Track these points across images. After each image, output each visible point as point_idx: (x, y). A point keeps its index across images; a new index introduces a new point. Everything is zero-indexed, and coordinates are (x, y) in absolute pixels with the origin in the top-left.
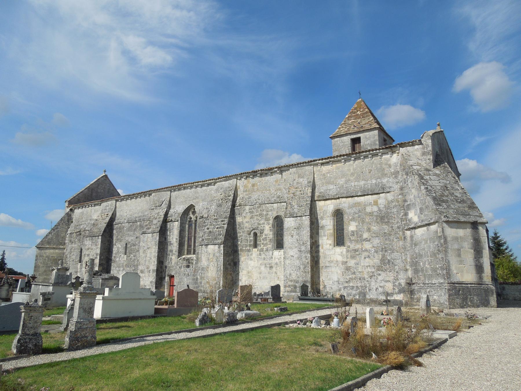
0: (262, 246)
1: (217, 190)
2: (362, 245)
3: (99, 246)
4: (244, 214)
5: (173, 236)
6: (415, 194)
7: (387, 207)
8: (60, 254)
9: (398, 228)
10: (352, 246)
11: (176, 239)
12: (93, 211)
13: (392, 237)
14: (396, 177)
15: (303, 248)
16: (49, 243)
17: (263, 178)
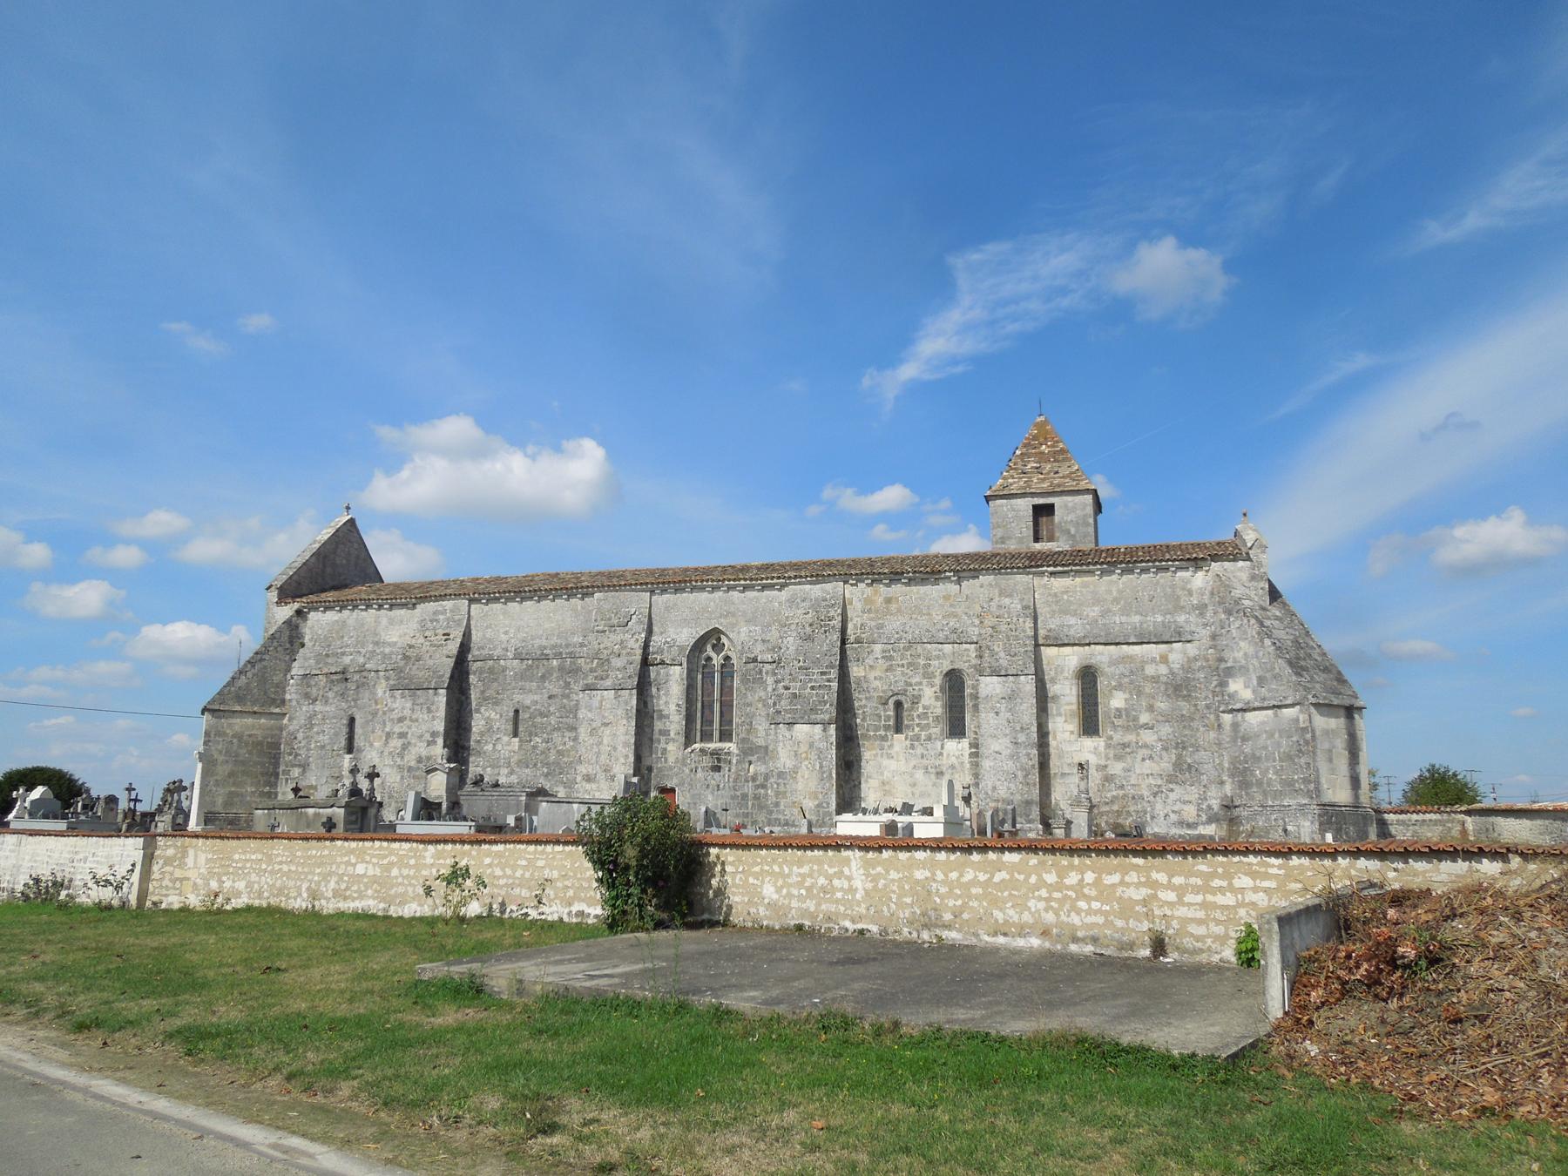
1: (791, 602)
3: (442, 713)
4: (869, 661)
5: (671, 696)
6: (1242, 647)
7: (1187, 669)
8: (271, 728)
9: (1208, 707)
10: (1118, 737)
12: (384, 621)
13: (1195, 724)
14: (1202, 614)
15: (1022, 738)
16: (240, 699)
17: (914, 589)
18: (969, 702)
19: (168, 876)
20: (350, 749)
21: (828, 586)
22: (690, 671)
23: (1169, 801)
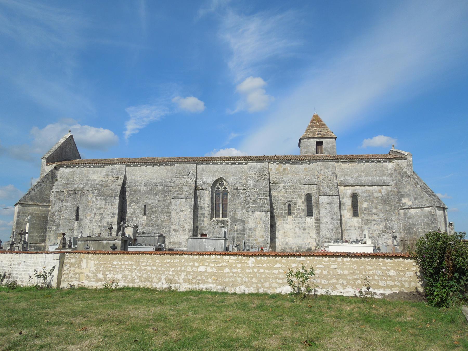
0: (296, 214)
1: (250, 169)
2: (372, 216)
4: (279, 190)
8: (44, 211)
9: (395, 207)
10: (365, 217)
11: (208, 204)
12: (91, 172)
13: (391, 213)
14: (391, 177)
15: (335, 217)
16: (32, 200)
17: (294, 166)
18: (314, 205)
19: (72, 272)
20: (77, 219)
21: (263, 164)
22: (212, 193)
23: (383, 239)
